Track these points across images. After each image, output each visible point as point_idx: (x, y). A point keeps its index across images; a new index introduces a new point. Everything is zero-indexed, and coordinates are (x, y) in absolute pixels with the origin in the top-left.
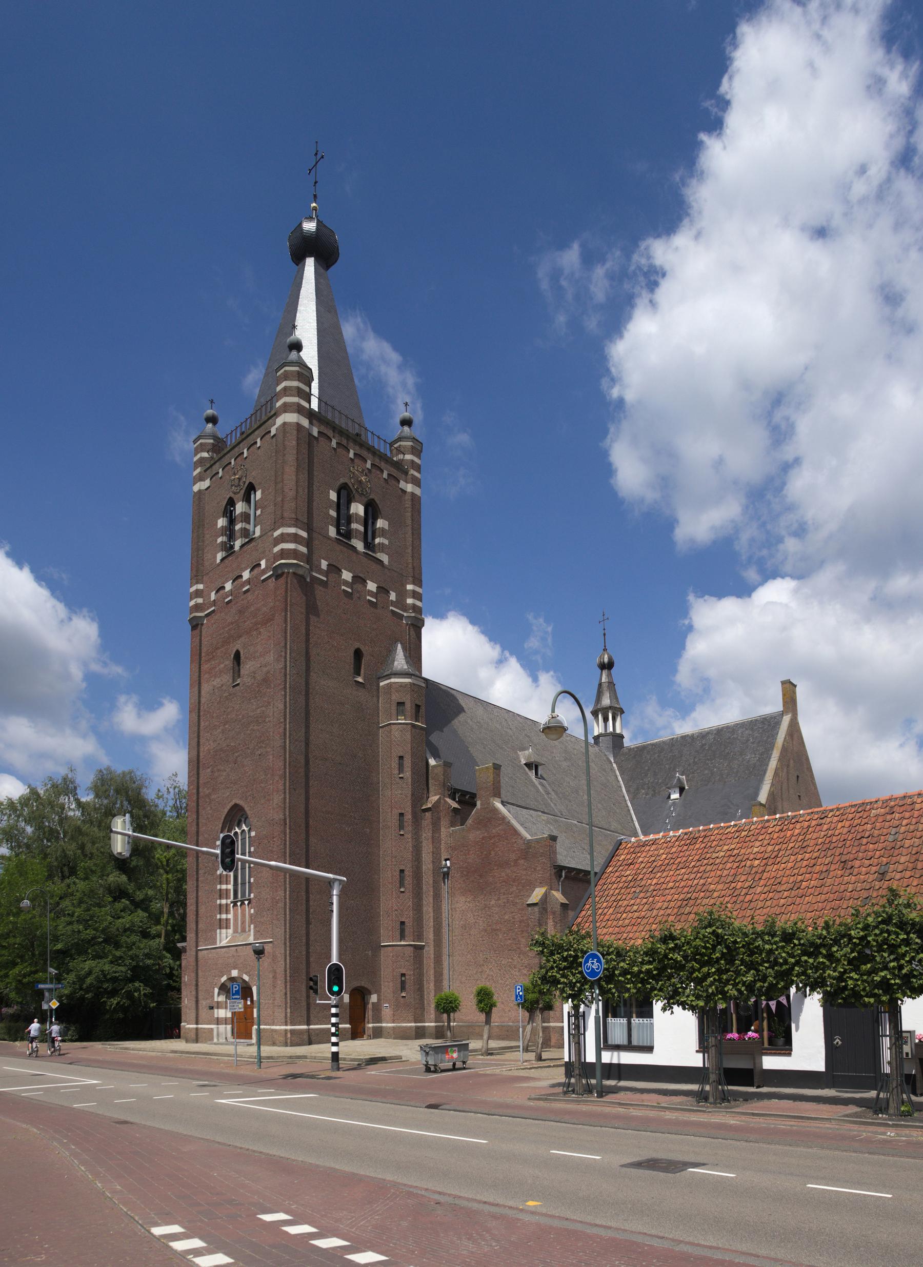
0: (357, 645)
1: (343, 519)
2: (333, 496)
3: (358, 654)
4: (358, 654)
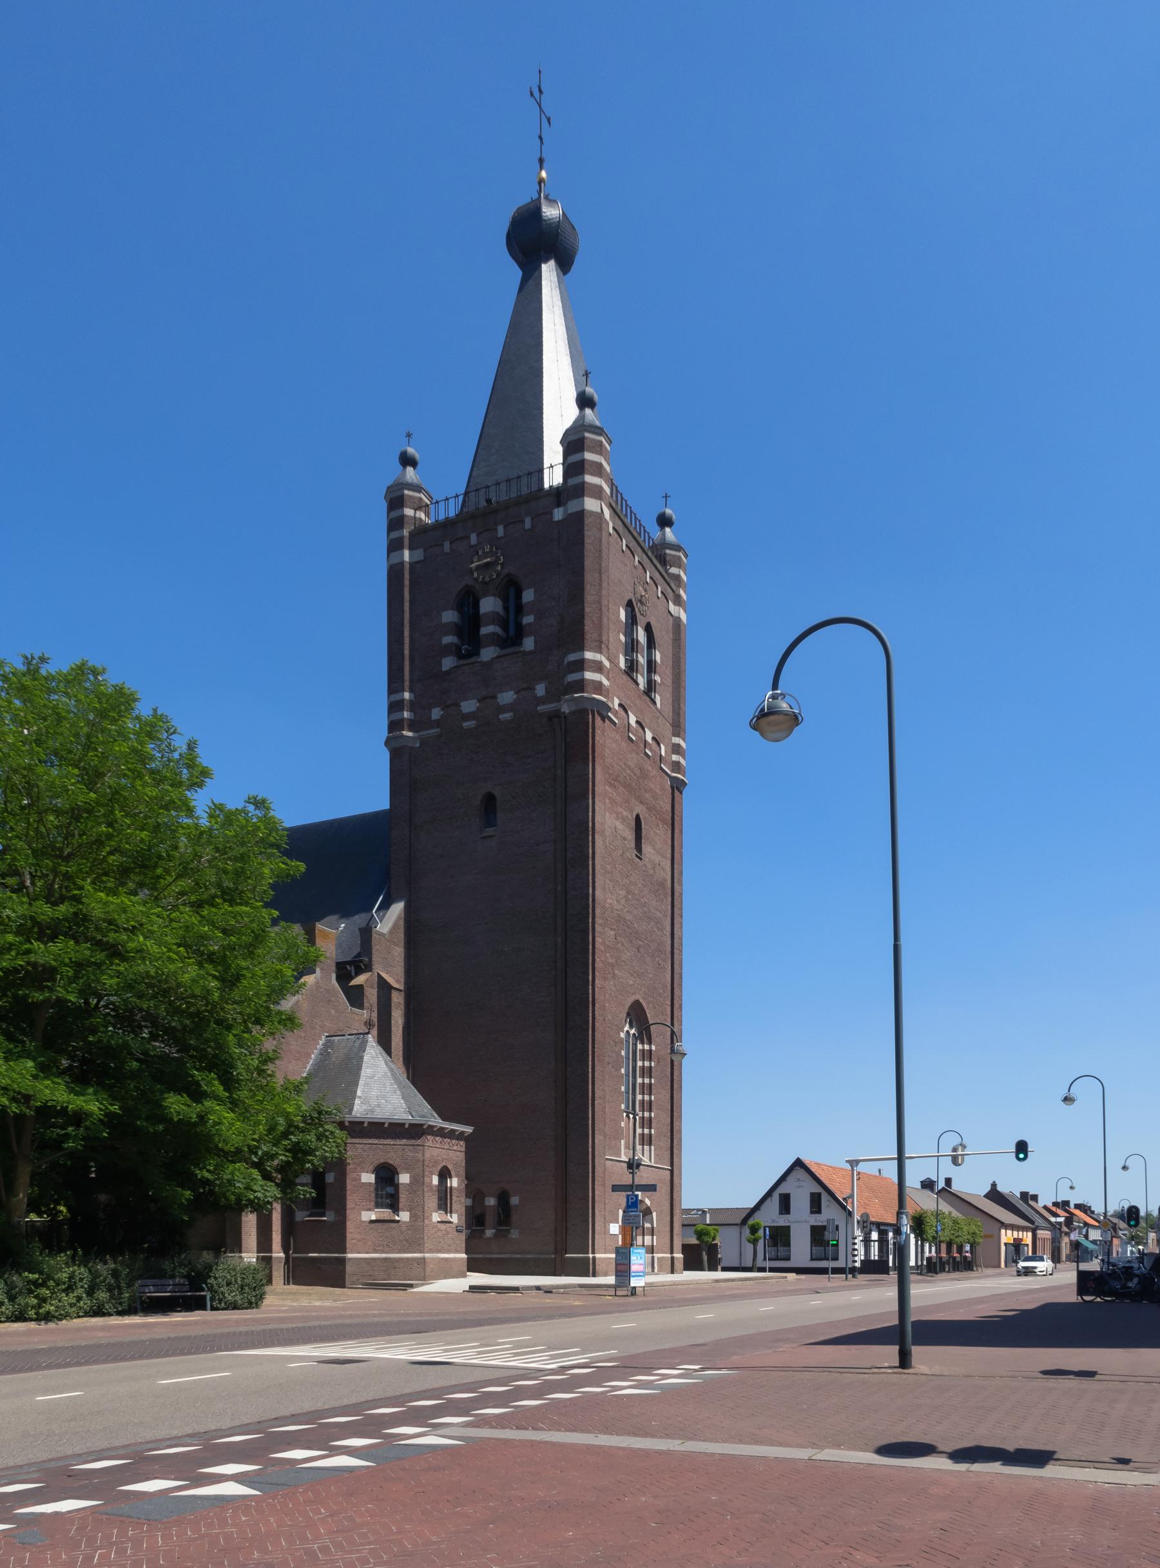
1: (631, 646)
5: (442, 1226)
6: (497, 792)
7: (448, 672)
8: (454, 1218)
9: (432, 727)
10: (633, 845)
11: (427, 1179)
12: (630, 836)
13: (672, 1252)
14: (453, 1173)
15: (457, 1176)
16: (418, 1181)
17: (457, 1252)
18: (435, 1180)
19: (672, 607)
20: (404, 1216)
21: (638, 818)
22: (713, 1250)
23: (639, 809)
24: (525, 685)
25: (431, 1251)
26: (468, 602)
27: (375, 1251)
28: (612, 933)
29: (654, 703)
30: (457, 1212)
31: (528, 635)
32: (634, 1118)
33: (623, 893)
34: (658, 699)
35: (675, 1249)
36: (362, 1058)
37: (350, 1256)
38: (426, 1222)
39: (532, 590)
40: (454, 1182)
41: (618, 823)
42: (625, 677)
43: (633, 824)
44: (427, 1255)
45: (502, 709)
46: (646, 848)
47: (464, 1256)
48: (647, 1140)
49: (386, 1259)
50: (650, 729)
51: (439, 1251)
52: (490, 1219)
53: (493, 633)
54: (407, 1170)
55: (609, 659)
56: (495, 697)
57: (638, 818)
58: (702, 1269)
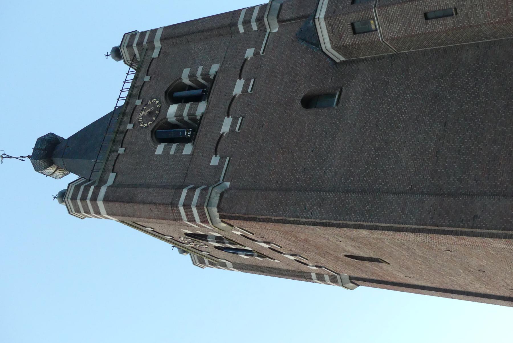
0: (298, 104)
2: (160, 149)
3: (308, 102)
4: (308, 102)
19: (155, 54)
34: (215, 68)
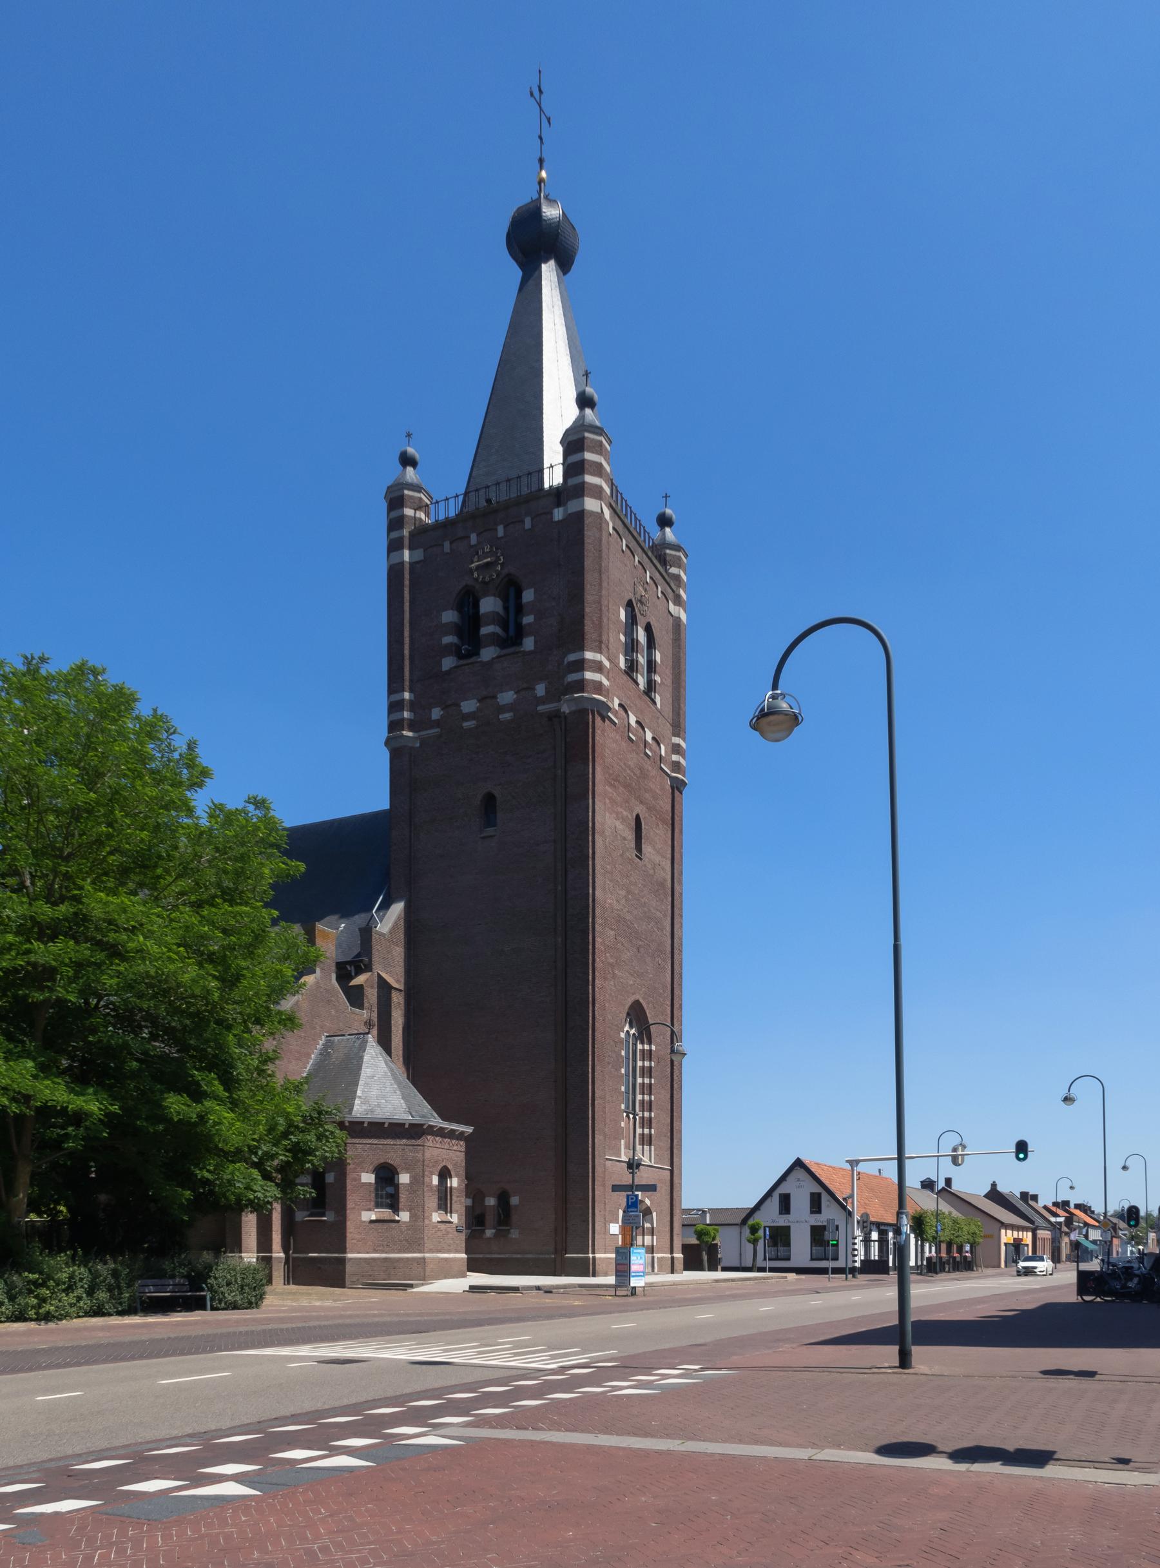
1: (631, 646)
5: (442, 1226)
6: (497, 792)
7: (448, 672)
8: (454, 1218)
9: (432, 727)
10: (633, 845)
11: (427, 1179)
12: (630, 836)
13: (672, 1252)
14: (453, 1173)
15: (457, 1176)
16: (418, 1181)
17: (457, 1252)
18: (435, 1180)
19: (672, 607)
20: (404, 1216)
21: (638, 818)
22: (713, 1250)
23: (639, 809)
24: (525, 685)
25: (431, 1251)
26: (468, 602)
27: (375, 1251)
28: (612, 933)
29: (654, 703)
30: (457, 1212)
31: (528, 635)
32: (634, 1118)
33: (623, 893)
34: (658, 699)
35: (675, 1249)
36: (362, 1058)
37: (350, 1256)
38: (426, 1222)
39: (532, 590)
40: (454, 1182)
41: (618, 823)
42: (625, 677)
43: (633, 824)
44: (427, 1255)
45: (502, 709)
46: (646, 848)
47: (464, 1256)
48: (647, 1140)
49: (386, 1259)
50: (650, 729)
51: (439, 1251)
52: (490, 1219)
53: (493, 633)
54: (407, 1170)
55: (609, 659)
56: (495, 697)
57: (638, 818)
58: (702, 1269)
